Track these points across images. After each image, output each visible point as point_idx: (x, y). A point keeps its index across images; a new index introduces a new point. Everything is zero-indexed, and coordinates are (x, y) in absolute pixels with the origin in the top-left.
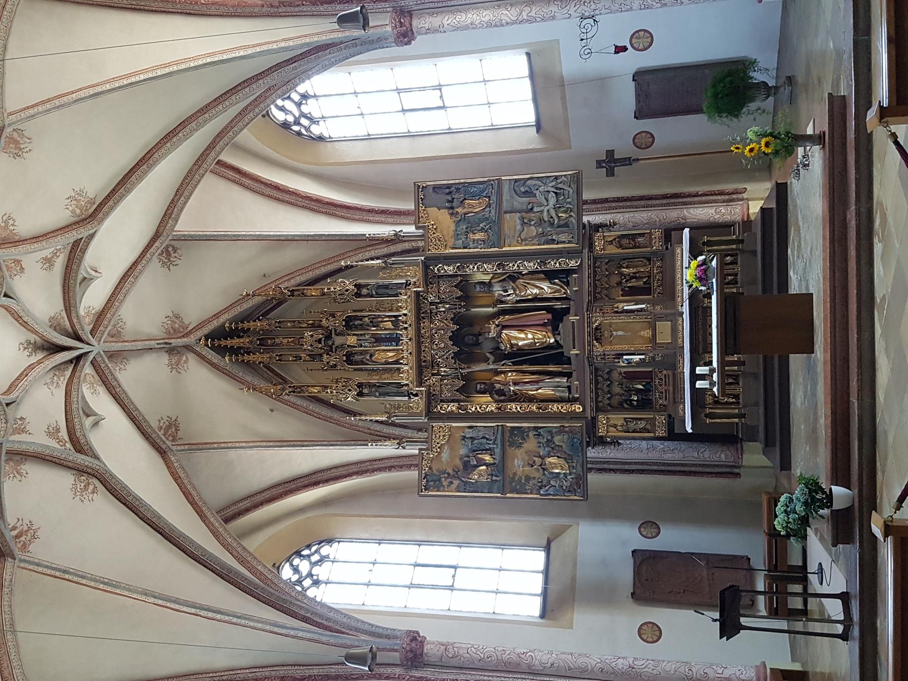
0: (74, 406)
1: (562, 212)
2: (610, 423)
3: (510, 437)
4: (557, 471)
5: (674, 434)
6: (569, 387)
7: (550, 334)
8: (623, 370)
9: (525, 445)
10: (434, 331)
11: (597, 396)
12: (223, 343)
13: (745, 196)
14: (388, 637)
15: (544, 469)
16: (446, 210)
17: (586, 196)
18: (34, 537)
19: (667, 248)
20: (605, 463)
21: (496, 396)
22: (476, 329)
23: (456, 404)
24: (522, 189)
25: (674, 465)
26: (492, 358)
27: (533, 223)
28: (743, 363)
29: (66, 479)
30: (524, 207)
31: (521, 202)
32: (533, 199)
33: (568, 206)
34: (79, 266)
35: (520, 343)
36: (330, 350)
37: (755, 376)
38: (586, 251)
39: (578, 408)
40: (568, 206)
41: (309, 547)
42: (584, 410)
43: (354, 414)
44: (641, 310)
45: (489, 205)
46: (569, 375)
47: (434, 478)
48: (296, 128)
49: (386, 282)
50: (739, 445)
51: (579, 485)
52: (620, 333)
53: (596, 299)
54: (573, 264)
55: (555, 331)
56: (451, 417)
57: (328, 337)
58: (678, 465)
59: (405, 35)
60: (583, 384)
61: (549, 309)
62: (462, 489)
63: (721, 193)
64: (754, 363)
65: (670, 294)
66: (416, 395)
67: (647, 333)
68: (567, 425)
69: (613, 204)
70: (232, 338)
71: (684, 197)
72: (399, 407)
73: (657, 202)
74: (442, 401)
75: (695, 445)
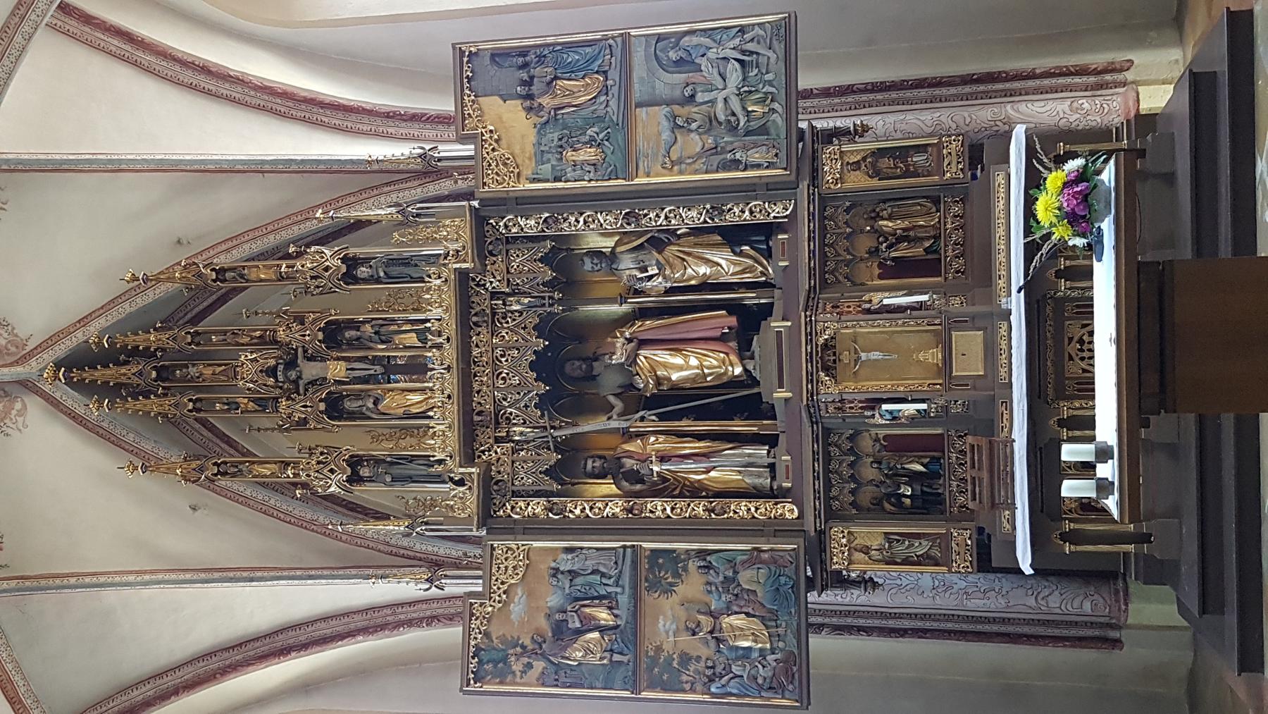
1: (757, 103)
3: (651, 570)
4: (746, 644)
6: (772, 467)
7: (733, 358)
8: (882, 432)
9: (680, 589)
10: (498, 352)
11: (828, 485)
12: (88, 375)
13: (1130, 76)
15: (718, 640)
16: (519, 102)
17: (804, 83)
19: (974, 177)
20: (848, 614)
21: (625, 484)
23: (543, 501)
24: (673, 55)
25: (988, 621)
26: (619, 405)
27: (694, 126)
30: (677, 93)
33: (768, 89)
35: (675, 377)
36: (294, 389)
37: (1173, 450)
39: (789, 511)
40: (768, 89)
44: (920, 306)
45: (605, 90)
46: (772, 441)
47: (495, 655)
49: (407, 251)
50: (1120, 584)
52: (875, 355)
53: (825, 285)
54: (778, 211)
55: (744, 350)
56: (532, 528)
57: (291, 364)
58: (994, 621)
61: (732, 308)
62: (550, 681)
63: (1082, 71)
65: (980, 271)
66: (461, 483)
67: (933, 356)
68: (765, 547)
69: (864, 97)
70: (106, 366)
71: (1007, 80)
73: (953, 90)
74: (515, 494)
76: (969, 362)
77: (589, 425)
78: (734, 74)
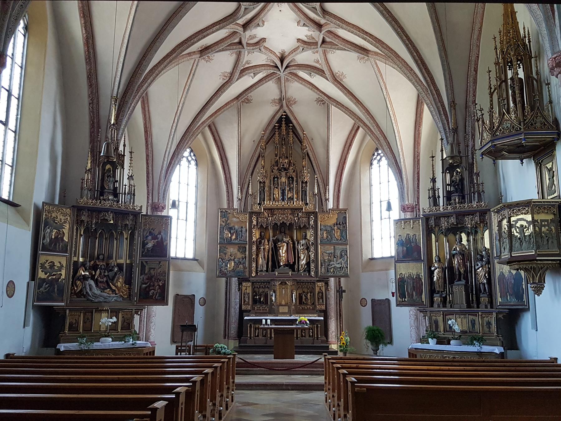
0: (258, 69)
2: (247, 287)
5: (242, 313)
6: (262, 271)
11: (258, 282)
14: (164, 197)
17: (342, 280)
18: (207, 61)
22: (287, 232)
26: (274, 239)
28: (271, 339)
29: (229, 69)
31: (338, 253)
32: (339, 258)
34: (315, 73)
35: (281, 251)
36: (279, 170)
38: (317, 279)
39: (254, 275)
41: (194, 155)
42: (253, 277)
43: (252, 175)
45: (337, 240)
46: (267, 271)
48: (376, 154)
51: (223, 274)
54: (312, 273)
55: (285, 265)
56: (251, 222)
57: (285, 169)
59: (404, 209)
60: (264, 277)
61: (294, 263)
64: (271, 343)
67: (283, 303)
72: (255, 199)
74: (257, 218)
75: (237, 321)
76: (281, 309)
77: (271, 231)
78: (338, 266)
